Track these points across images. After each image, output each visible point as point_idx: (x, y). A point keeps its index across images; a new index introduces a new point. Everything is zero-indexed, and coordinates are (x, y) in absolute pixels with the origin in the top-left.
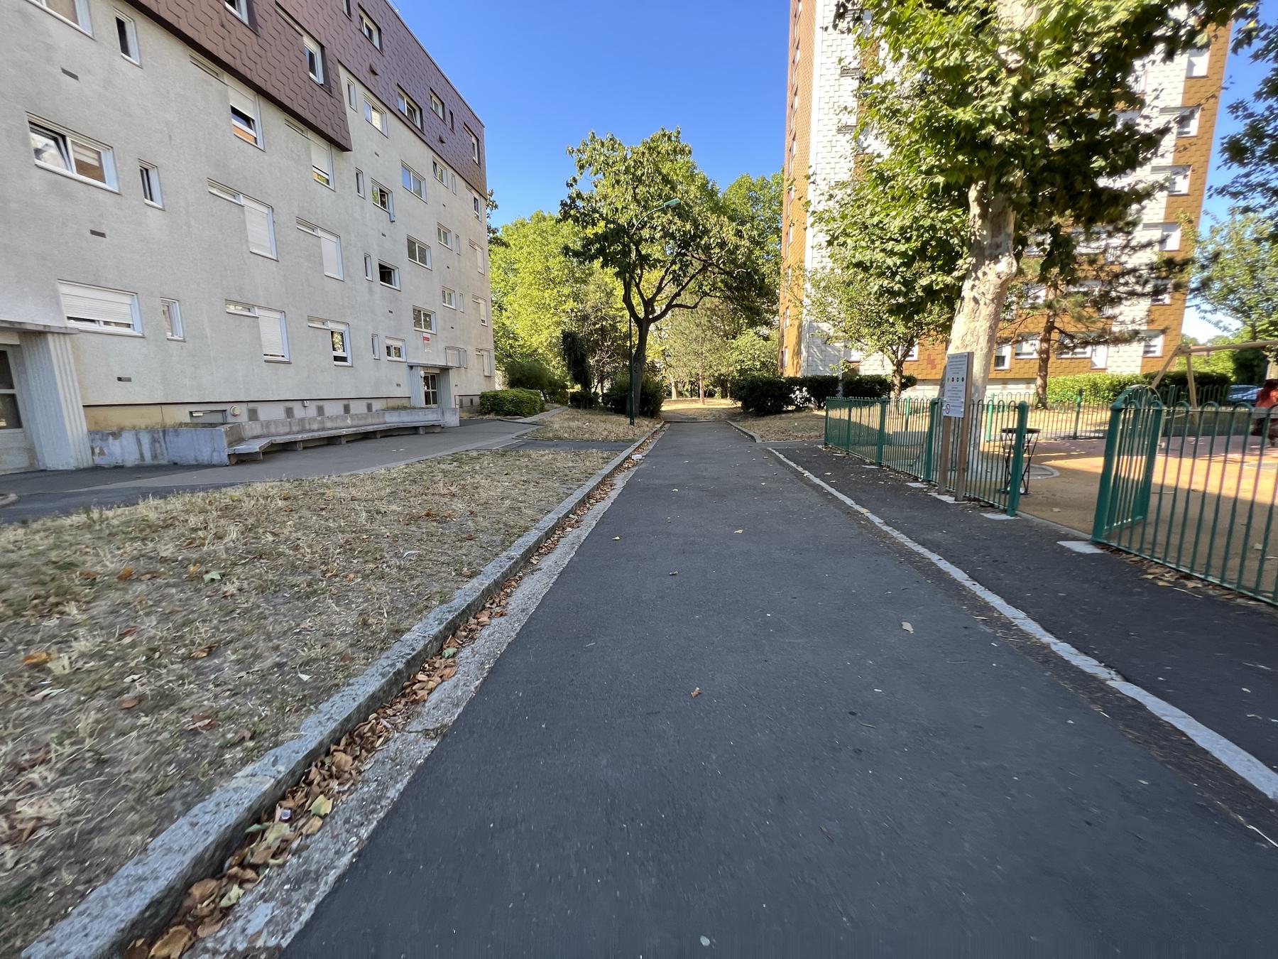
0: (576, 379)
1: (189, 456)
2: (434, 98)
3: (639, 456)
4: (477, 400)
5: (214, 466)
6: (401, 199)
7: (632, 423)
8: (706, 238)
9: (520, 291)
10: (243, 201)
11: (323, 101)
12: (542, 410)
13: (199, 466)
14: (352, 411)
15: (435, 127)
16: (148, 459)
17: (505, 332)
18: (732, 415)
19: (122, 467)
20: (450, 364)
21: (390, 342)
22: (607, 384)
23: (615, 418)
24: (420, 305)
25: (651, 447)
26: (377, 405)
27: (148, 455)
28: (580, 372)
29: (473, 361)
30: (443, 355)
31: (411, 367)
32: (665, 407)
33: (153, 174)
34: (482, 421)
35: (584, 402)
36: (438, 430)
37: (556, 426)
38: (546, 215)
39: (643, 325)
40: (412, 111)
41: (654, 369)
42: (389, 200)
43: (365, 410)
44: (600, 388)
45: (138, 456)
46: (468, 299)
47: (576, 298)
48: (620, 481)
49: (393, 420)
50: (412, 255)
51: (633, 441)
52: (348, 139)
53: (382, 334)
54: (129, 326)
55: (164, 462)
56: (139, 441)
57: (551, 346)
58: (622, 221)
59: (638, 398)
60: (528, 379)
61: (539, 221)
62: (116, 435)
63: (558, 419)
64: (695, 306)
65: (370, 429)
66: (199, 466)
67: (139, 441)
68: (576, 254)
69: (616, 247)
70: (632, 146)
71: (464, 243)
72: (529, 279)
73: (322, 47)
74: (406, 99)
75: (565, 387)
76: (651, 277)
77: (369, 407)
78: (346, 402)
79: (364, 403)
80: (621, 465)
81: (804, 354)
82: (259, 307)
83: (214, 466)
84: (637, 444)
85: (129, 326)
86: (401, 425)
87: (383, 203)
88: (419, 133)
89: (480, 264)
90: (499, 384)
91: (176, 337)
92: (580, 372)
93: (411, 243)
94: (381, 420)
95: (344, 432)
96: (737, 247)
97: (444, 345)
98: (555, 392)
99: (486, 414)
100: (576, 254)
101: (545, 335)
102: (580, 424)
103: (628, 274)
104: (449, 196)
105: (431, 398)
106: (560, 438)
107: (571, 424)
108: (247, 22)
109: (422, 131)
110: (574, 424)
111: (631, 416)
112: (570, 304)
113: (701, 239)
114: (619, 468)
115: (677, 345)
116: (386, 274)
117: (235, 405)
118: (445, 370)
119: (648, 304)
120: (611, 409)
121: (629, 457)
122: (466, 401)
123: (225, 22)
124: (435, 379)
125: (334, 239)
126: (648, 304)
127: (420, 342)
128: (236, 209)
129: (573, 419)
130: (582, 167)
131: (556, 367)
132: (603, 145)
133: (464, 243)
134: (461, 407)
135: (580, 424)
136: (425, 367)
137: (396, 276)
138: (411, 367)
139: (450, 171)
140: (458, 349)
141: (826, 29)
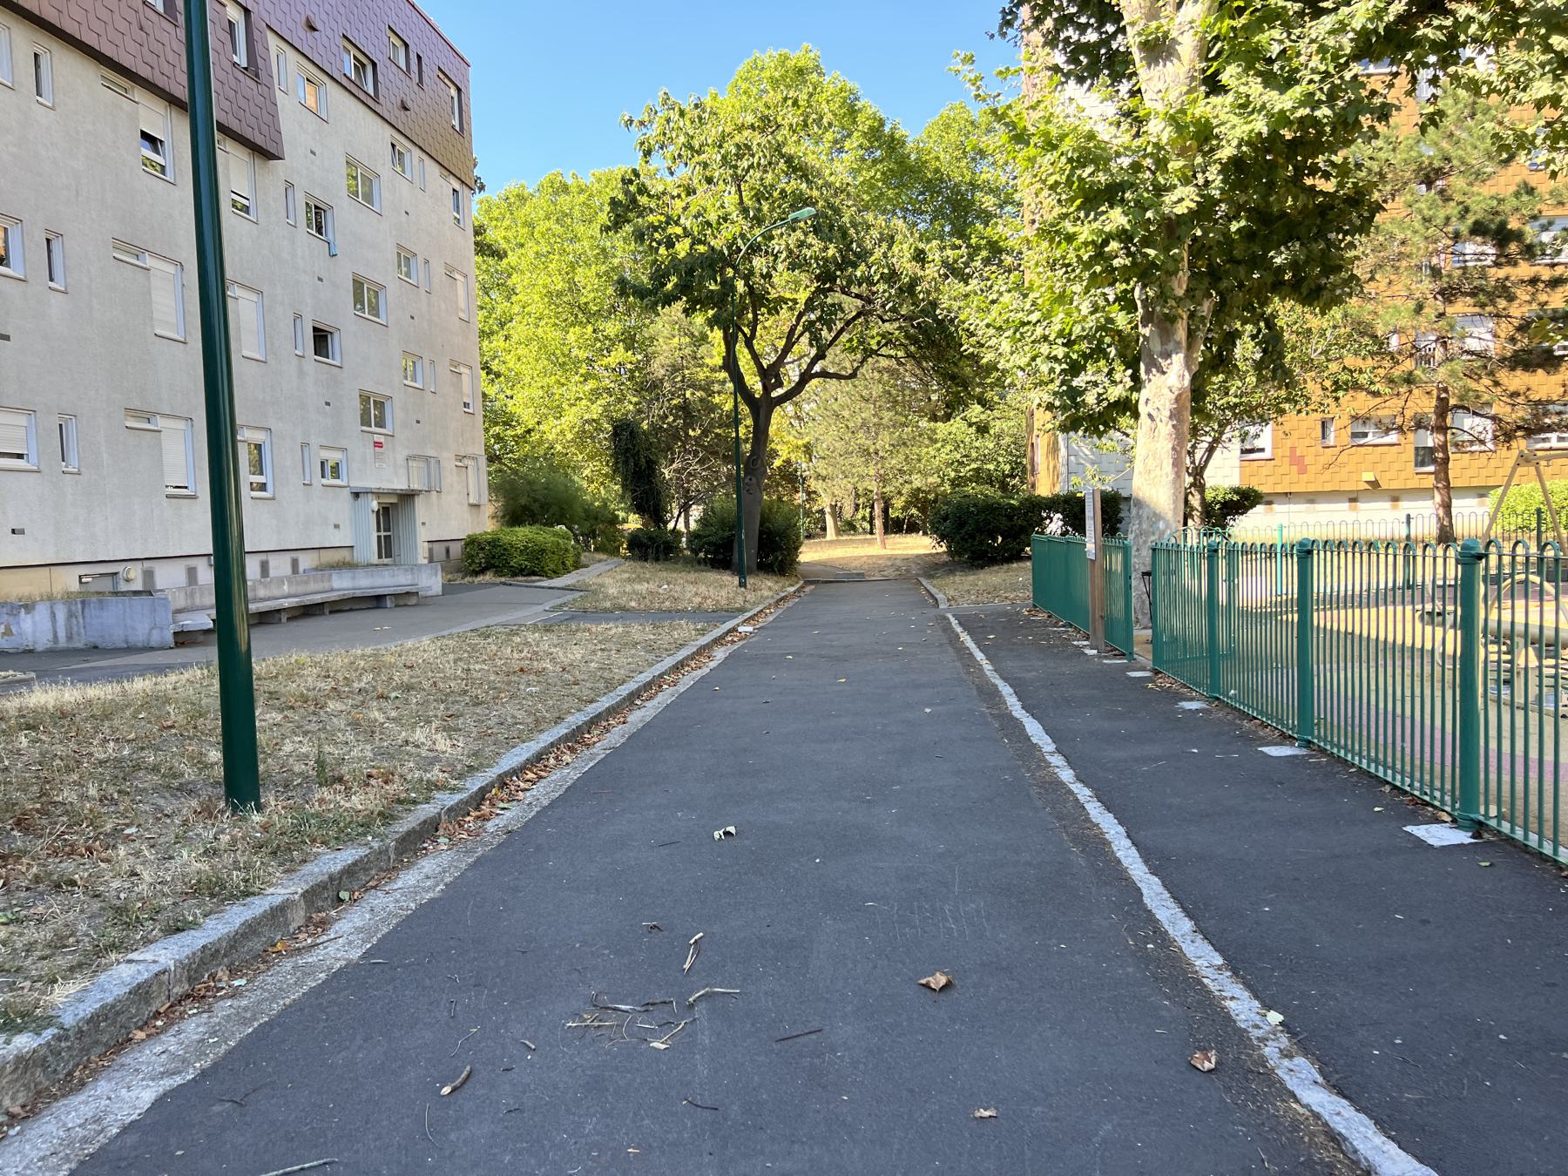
0: (639, 508)
1: (117, 637)
2: (394, 39)
3: (750, 629)
4: (456, 549)
5: (152, 649)
6: (345, 215)
7: (742, 585)
8: (863, 267)
9: (518, 330)
10: (149, 262)
11: (248, 93)
12: (577, 565)
13: (130, 649)
14: (272, 573)
15: (394, 84)
16: (63, 643)
17: (498, 418)
18: (931, 567)
19: (31, 651)
20: (415, 486)
21: (325, 454)
22: (696, 512)
23: (713, 576)
24: (369, 387)
25: (771, 618)
26: (306, 561)
27: (62, 634)
28: (648, 500)
29: (451, 478)
30: (402, 471)
31: (356, 495)
32: (809, 554)
33: (55, 245)
34: (470, 587)
35: (653, 548)
36: (413, 601)
37: (612, 591)
38: (570, 181)
39: (762, 409)
40: (360, 67)
41: (791, 477)
42: (332, 222)
43: (289, 571)
44: (684, 521)
45: (51, 637)
46: (444, 369)
47: (629, 341)
48: (720, 654)
49: (343, 584)
50: (358, 298)
51: (742, 610)
52: (279, 143)
53: (315, 442)
54: (20, 456)
55: (79, 645)
56: (53, 615)
57: (582, 436)
58: (718, 243)
59: (757, 541)
60: (545, 507)
61: (556, 193)
62: (29, 607)
63: (611, 578)
64: (853, 375)
65: (318, 598)
66: (130, 649)
67: (53, 615)
68: (641, 293)
69: (708, 283)
70: (730, 104)
71: (438, 269)
72: (538, 306)
73: (247, 11)
74: (353, 51)
75: (614, 521)
76: (771, 331)
77: (295, 563)
78: (263, 557)
79: (288, 557)
80: (722, 637)
81: (1063, 452)
82: (163, 415)
83: (152, 649)
84: (748, 615)
85: (20, 456)
86: (358, 593)
87: (319, 230)
88: (371, 103)
89: (462, 304)
90: (485, 524)
91: (70, 469)
92: (648, 500)
93: (358, 285)
94: (326, 586)
95: (286, 603)
96: (915, 281)
97: (406, 453)
98: (596, 529)
99: (476, 573)
100: (641, 293)
101: (571, 417)
102: (652, 586)
103: (733, 322)
104: (416, 192)
105: (386, 547)
106: (623, 609)
107: (637, 587)
108: (161, 10)
109: (376, 99)
110: (643, 587)
111: (742, 573)
112: (619, 354)
113: (855, 266)
114: (718, 641)
115: (827, 436)
116: (321, 339)
117: (129, 565)
118: (408, 497)
119: (770, 375)
120: (705, 561)
121: (734, 630)
122: (439, 550)
123: (144, 22)
124: (394, 511)
125: (254, 297)
126: (770, 375)
127: (370, 449)
128: (140, 274)
129: (640, 580)
130: (648, 153)
131: (595, 481)
132: (682, 114)
133: (438, 269)
134: (431, 560)
135: (652, 586)
136: (378, 494)
137: (335, 343)
138: (356, 495)
139: (417, 152)
140: (427, 459)
141: (992, 36)
